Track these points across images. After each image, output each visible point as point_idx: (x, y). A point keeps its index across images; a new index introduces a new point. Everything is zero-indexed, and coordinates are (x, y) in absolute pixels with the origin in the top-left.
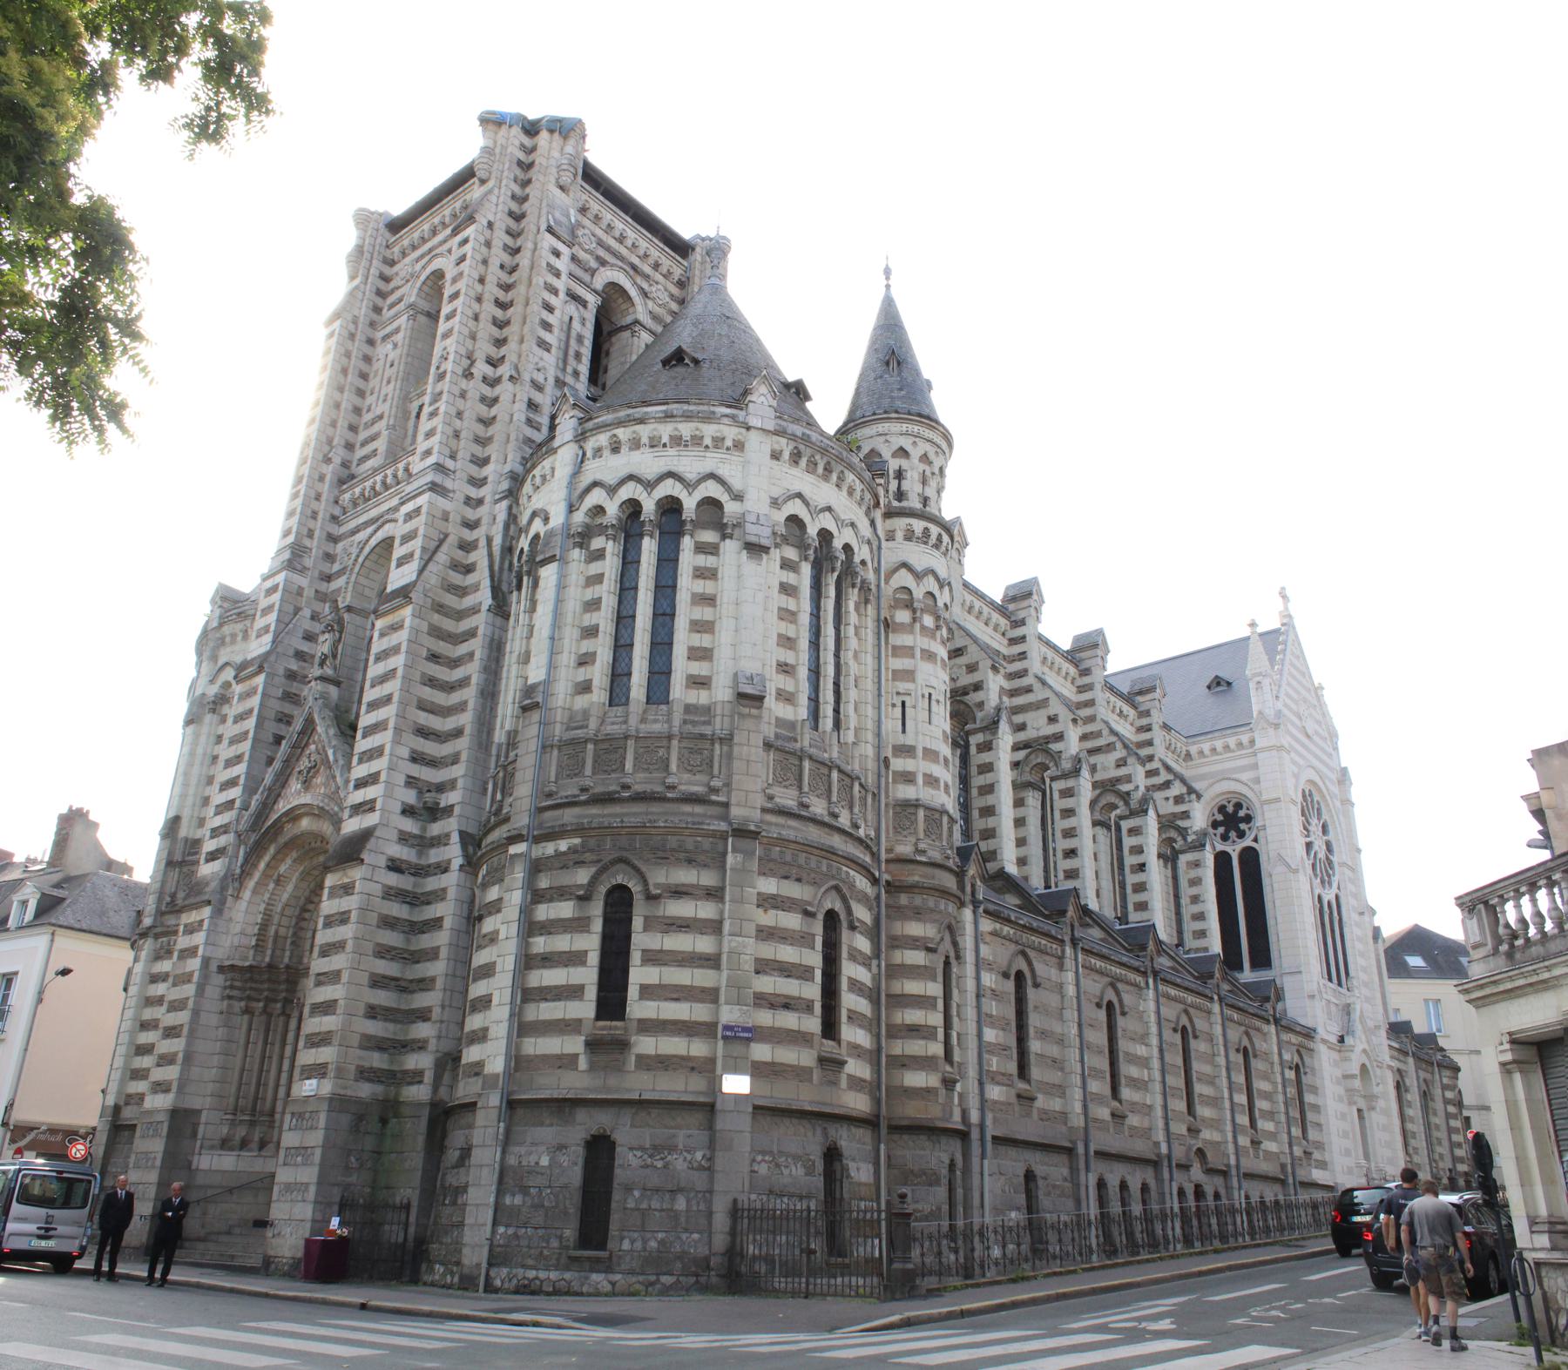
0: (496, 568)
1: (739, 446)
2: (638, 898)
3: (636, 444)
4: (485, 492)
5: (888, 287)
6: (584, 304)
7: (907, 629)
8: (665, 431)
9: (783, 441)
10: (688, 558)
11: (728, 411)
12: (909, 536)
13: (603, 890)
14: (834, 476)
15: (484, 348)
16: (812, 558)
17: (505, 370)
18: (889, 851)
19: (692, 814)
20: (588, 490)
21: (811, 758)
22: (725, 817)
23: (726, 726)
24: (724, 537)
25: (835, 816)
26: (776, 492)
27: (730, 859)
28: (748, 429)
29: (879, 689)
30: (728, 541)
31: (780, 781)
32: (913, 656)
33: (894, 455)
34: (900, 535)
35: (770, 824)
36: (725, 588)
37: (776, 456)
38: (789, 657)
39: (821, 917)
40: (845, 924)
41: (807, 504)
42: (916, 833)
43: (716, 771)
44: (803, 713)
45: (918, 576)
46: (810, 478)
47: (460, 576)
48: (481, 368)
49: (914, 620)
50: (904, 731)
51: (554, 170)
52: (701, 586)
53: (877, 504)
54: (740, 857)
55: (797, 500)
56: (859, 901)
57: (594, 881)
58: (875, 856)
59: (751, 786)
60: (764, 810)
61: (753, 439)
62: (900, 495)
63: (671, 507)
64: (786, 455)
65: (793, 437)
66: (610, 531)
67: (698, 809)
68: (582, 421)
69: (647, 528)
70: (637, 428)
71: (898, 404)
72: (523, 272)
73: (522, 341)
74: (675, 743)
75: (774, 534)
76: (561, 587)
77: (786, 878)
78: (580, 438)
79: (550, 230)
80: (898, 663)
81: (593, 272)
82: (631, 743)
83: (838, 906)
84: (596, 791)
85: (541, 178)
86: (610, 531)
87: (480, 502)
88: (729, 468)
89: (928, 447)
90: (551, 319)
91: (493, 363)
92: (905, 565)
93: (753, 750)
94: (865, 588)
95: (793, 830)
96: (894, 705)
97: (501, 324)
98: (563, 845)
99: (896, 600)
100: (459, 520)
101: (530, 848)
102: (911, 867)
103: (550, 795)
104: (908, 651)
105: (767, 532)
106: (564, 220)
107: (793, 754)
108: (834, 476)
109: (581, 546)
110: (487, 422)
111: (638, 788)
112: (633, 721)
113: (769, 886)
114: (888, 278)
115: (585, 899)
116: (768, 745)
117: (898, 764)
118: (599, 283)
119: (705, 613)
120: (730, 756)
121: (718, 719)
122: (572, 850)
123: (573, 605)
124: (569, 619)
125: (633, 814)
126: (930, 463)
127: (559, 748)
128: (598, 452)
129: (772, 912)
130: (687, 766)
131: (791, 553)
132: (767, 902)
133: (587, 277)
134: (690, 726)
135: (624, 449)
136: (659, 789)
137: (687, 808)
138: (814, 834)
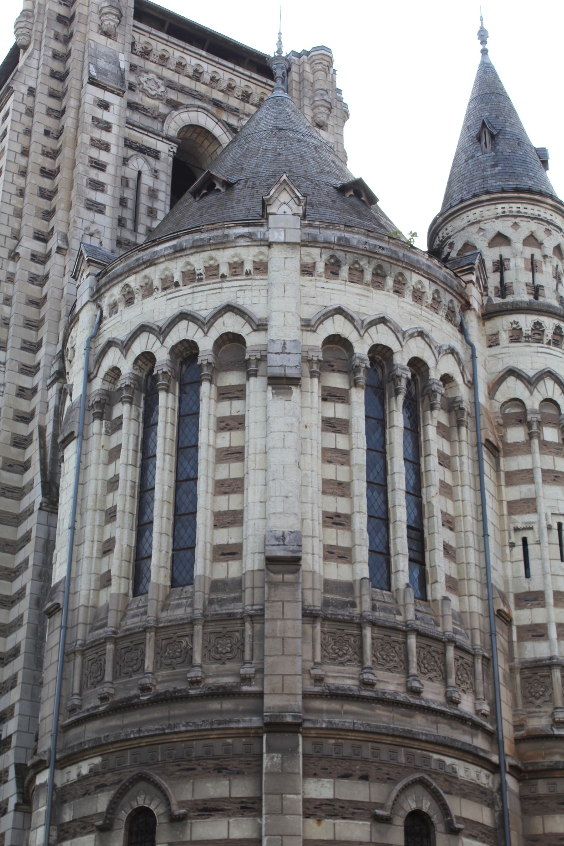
0: (48, 460)
1: (261, 268)
2: (161, 820)
3: (148, 290)
4: (38, 379)
5: (484, 52)
6: (155, 155)
7: (524, 448)
8: (176, 268)
9: (315, 251)
11: (246, 230)
12: (516, 336)
13: (123, 815)
14: (390, 282)
16: (362, 382)
17: (54, 243)
18: (518, 727)
19: (220, 712)
20: (104, 353)
21: (374, 624)
22: (259, 711)
23: (257, 600)
24: (250, 374)
25: (416, 692)
26: (310, 312)
27: (266, 762)
28: (270, 245)
29: (485, 528)
30: (252, 379)
31: (332, 656)
32: (532, 481)
33: (492, 244)
34: (504, 337)
35: (320, 711)
36: (253, 437)
37: (307, 270)
38: (340, 505)
39: (399, 821)
40: (440, 827)
41: (350, 318)
42: (551, 699)
43: (247, 656)
45: (531, 383)
46: (357, 288)
47: (15, 477)
48: (29, 245)
49: (531, 436)
50: (528, 575)
51: (95, 17)
52: (226, 440)
53: (467, 306)
54: (277, 758)
56: (465, 796)
57: (113, 806)
58: (493, 736)
59: (290, 665)
60: (306, 696)
61: (276, 257)
62: (504, 289)
63: (186, 352)
64: (320, 267)
65: (326, 245)
66: (125, 394)
67: (228, 705)
68: (98, 276)
69: (162, 381)
70: (147, 271)
72: (68, 134)
74: (198, 628)
75: (310, 361)
76: (81, 468)
77: (346, 776)
79: (93, 82)
80: (514, 493)
81: (162, 118)
83: (427, 805)
84: (118, 698)
85: (82, 28)
86: (125, 394)
87: (34, 391)
88: (250, 295)
89: (533, 226)
90: (102, 177)
92: (512, 372)
93: (289, 623)
94: (453, 407)
95: (350, 716)
96: (512, 545)
98: (85, 768)
99: (506, 417)
102: (549, 744)
103: (73, 710)
104: (526, 476)
105: (295, 360)
106: (110, 67)
107: (349, 622)
108: (390, 282)
109: (100, 416)
110: (38, 303)
111: (160, 688)
112: (152, 611)
113: (322, 789)
114: (484, 42)
116: (310, 616)
117: (523, 617)
118: (173, 127)
119: (231, 470)
120: (262, 636)
121: (248, 592)
122: (94, 772)
123: (94, 486)
124: (90, 503)
125: (150, 720)
126: (540, 245)
127: (83, 653)
128: (114, 307)
129: (328, 822)
130: (213, 654)
132: (315, 809)
133: (156, 125)
135: (138, 298)
136: (182, 686)
137: (215, 705)
138: (382, 717)
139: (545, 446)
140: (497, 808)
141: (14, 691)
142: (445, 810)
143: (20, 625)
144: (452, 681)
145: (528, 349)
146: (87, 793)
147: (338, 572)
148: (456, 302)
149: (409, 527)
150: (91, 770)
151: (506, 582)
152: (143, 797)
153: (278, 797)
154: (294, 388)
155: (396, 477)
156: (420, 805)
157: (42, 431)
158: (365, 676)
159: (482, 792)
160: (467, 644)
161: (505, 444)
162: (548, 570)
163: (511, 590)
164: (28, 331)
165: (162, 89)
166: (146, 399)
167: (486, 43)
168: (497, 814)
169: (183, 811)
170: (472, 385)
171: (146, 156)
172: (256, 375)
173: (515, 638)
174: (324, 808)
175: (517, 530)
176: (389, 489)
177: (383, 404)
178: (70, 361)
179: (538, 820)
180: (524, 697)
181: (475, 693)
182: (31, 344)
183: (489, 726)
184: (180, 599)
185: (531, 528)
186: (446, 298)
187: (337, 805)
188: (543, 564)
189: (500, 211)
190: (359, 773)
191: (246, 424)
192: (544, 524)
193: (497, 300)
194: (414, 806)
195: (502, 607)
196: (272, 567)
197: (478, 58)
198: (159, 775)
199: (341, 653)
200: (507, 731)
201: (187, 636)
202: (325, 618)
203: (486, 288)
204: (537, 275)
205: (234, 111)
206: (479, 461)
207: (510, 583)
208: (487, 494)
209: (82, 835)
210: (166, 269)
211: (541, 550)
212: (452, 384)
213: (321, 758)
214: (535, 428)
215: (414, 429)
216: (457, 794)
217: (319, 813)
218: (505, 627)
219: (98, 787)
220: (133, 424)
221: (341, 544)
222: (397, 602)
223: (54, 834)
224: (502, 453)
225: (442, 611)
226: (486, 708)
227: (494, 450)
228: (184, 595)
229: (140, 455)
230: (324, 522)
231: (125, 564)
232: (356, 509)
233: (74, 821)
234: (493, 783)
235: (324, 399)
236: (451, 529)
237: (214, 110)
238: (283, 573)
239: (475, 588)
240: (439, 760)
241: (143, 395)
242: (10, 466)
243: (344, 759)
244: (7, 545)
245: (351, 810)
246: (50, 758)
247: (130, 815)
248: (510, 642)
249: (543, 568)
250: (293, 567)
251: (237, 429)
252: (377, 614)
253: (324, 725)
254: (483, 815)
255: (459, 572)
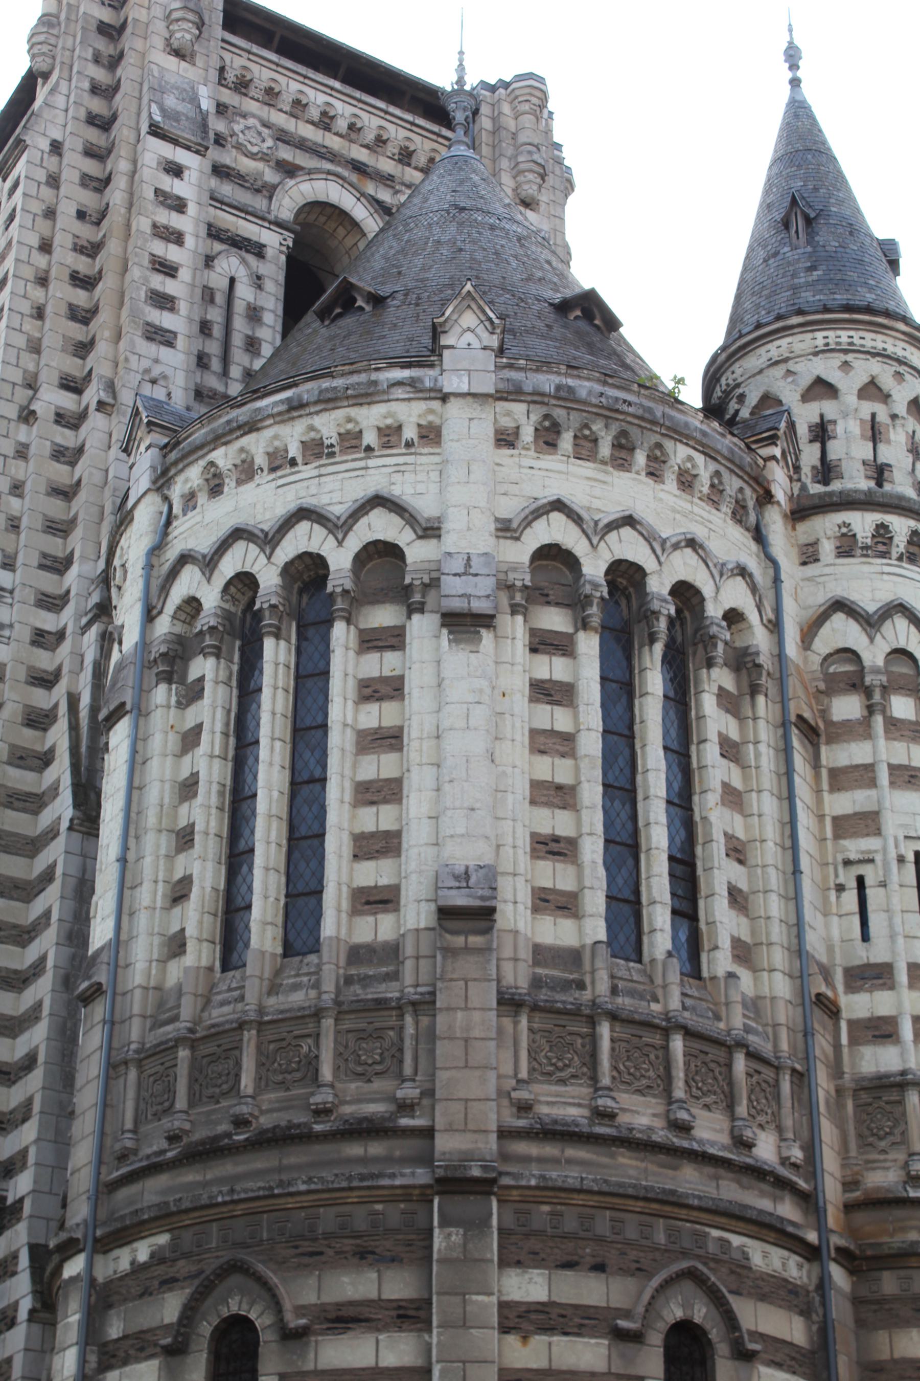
0: (83, 749)
1: (431, 435)
2: (267, 1336)
3: (247, 471)
4: (67, 617)
5: (795, 83)
6: (258, 250)
7: (860, 729)
8: (291, 437)
9: (519, 408)
10: (346, 663)
11: (406, 373)
12: (847, 547)
13: (206, 1329)
14: (640, 458)
15: (57, 361)
16: (596, 621)
17: (93, 394)
18: (849, 1185)
19: (364, 1160)
20: (173, 573)
21: (614, 1017)
22: (427, 1159)
25: (684, 1128)
26: (510, 508)
28: (445, 398)
30: (416, 617)
32: (873, 783)
33: (807, 396)
34: (827, 548)
35: (526, 1160)
36: (417, 712)
37: (506, 439)
38: (559, 823)
39: (656, 1339)
40: (722, 1349)
43: (408, 1070)
44: (596, 929)
45: (871, 623)
46: (586, 469)
47: (30, 776)
48: (51, 398)
49: (870, 710)
50: (865, 937)
52: (372, 716)
53: (766, 498)
54: (457, 1235)
55: (556, 516)
56: (763, 1297)
58: (809, 1200)
59: (477, 1084)
60: (504, 1134)
62: (827, 471)
63: (308, 573)
64: (527, 434)
65: (537, 398)
66: (208, 641)
67: (376, 1148)
70: (245, 441)
71: (808, 297)
72: (116, 217)
73: (119, 337)
74: (328, 1023)
77: (569, 1265)
78: (162, 480)
79: (156, 131)
81: (269, 191)
82: (249, 1037)
83: (701, 1313)
84: (197, 1136)
85: (139, 44)
86: (208, 641)
87: (61, 635)
88: (413, 481)
89: (875, 367)
90: (170, 287)
91: (73, 385)
92: (840, 606)
93: (477, 1016)
94: (743, 662)
95: (575, 1166)
96: (840, 888)
97: (82, 316)
98: (142, 1251)
100: (22, 675)
101: (90, 1265)
102: (899, 1213)
103: (123, 1157)
104: (863, 775)
105: (485, 585)
107: (574, 1013)
108: (640, 458)
109: (168, 678)
110: (66, 493)
111: (266, 1121)
112: (252, 996)
113: (530, 1286)
114: (794, 67)
115: (176, 1350)
116: (509, 1003)
117: (858, 1005)
118: (287, 205)
119: (381, 766)
120: (432, 1036)
121: (409, 965)
122: (158, 1258)
123: (157, 793)
125: (249, 1173)
127: (139, 1063)
128: (190, 499)
129: (539, 1341)
130: (352, 1066)
131: (555, 620)
132: (519, 1319)
133: (258, 203)
134: (357, 989)
135: (229, 485)
136: (300, 1118)
137: (355, 1149)
138: (628, 1169)
139: (894, 726)
140: (815, 1317)
141: (27, 1125)
142: (730, 1320)
143: (38, 1019)
144: (742, 1110)
145: (866, 568)
146: (146, 1293)
147: (557, 932)
148: (748, 492)
149: (671, 858)
150: (152, 1255)
151: (830, 949)
152: (237, 1298)
153: (458, 1299)
154: (484, 632)
155: (651, 776)
156: (689, 1313)
157: (73, 701)
158: (600, 1102)
159: (790, 1292)
160: (766, 1049)
161: (829, 723)
162: (899, 929)
163: (838, 960)
164: (50, 538)
165: (270, 143)
166: (242, 650)
167: (798, 68)
168: (815, 1328)
169: (303, 1321)
170: (775, 626)
171: (243, 253)
172: (422, 611)
173: (844, 1040)
174: (533, 1316)
175: (847, 863)
176: (640, 797)
177: (629, 658)
178: (119, 588)
179: (882, 1337)
180: (860, 1136)
181: (780, 1129)
182: (55, 559)
183: (802, 1184)
184: (297, 975)
185: (872, 861)
186: (732, 484)
187: (555, 1312)
188: (890, 919)
189: (820, 342)
190: (589, 1260)
191: (406, 690)
192: (893, 854)
193: (816, 489)
194: (679, 1314)
195: (823, 989)
196: (449, 924)
197: (785, 92)
198: (263, 1262)
199: (560, 1064)
200: (832, 1192)
201: (309, 1036)
202: (535, 1008)
203: (797, 469)
204: (881, 447)
205: (387, 180)
206: (786, 752)
207: (837, 950)
208: (799, 805)
209: (138, 1360)
210: (276, 437)
211: (888, 897)
212: (742, 626)
213: (527, 1235)
214: (877, 697)
215: (680, 699)
216: (750, 1295)
217: (525, 1325)
218: (829, 1023)
219: (163, 1283)
220: (222, 690)
221: (561, 886)
222: (652, 981)
223: (93, 1359)
224: (823, 739)
225: (726, 996)
226: (797, 1154)
227: (811, 733)
228: (305, 970)
229: (232, 741)
230: (533, 850)
231: (208, 918)
232: (586, 829)
233: (125, 1337)
234: (809, 1277)
235: (534, 650)
236: (741, 862)
237: (354, 177)
238: (467, 933)
239: (779, 957)
240: (721, 1239)
241: (238, 643)
242: (21, 758)
243: (564, 1237)
244: (16, 887)
245: (577, 1320)
246: (85, 1236)
247: (216, 1328)
248: (837, 1046)
249: (891, 926)
250: (483, 924)
251: (392, 698)
252: (620, 1000)
253: (533, 1182)
254: (793, 1329)
255: (753, 933)
